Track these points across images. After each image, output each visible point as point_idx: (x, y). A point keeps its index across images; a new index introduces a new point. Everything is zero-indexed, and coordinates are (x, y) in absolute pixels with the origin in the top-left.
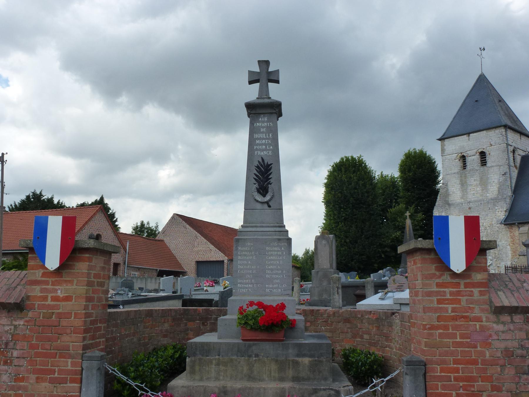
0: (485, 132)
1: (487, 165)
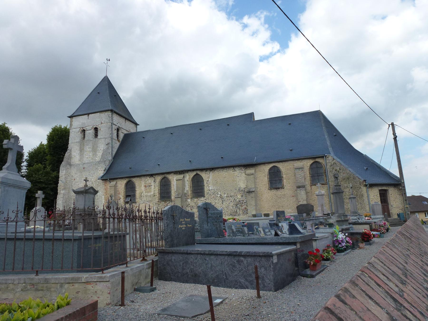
0: (98, 114)
1: (98, 137)
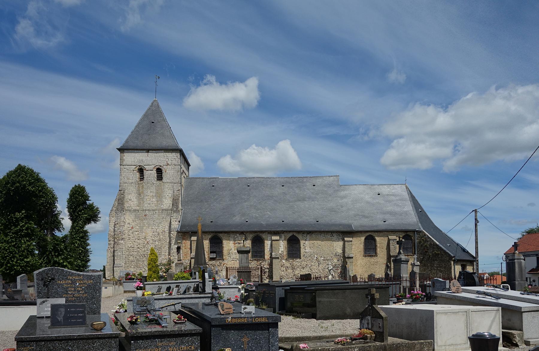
1: (163, 181)
